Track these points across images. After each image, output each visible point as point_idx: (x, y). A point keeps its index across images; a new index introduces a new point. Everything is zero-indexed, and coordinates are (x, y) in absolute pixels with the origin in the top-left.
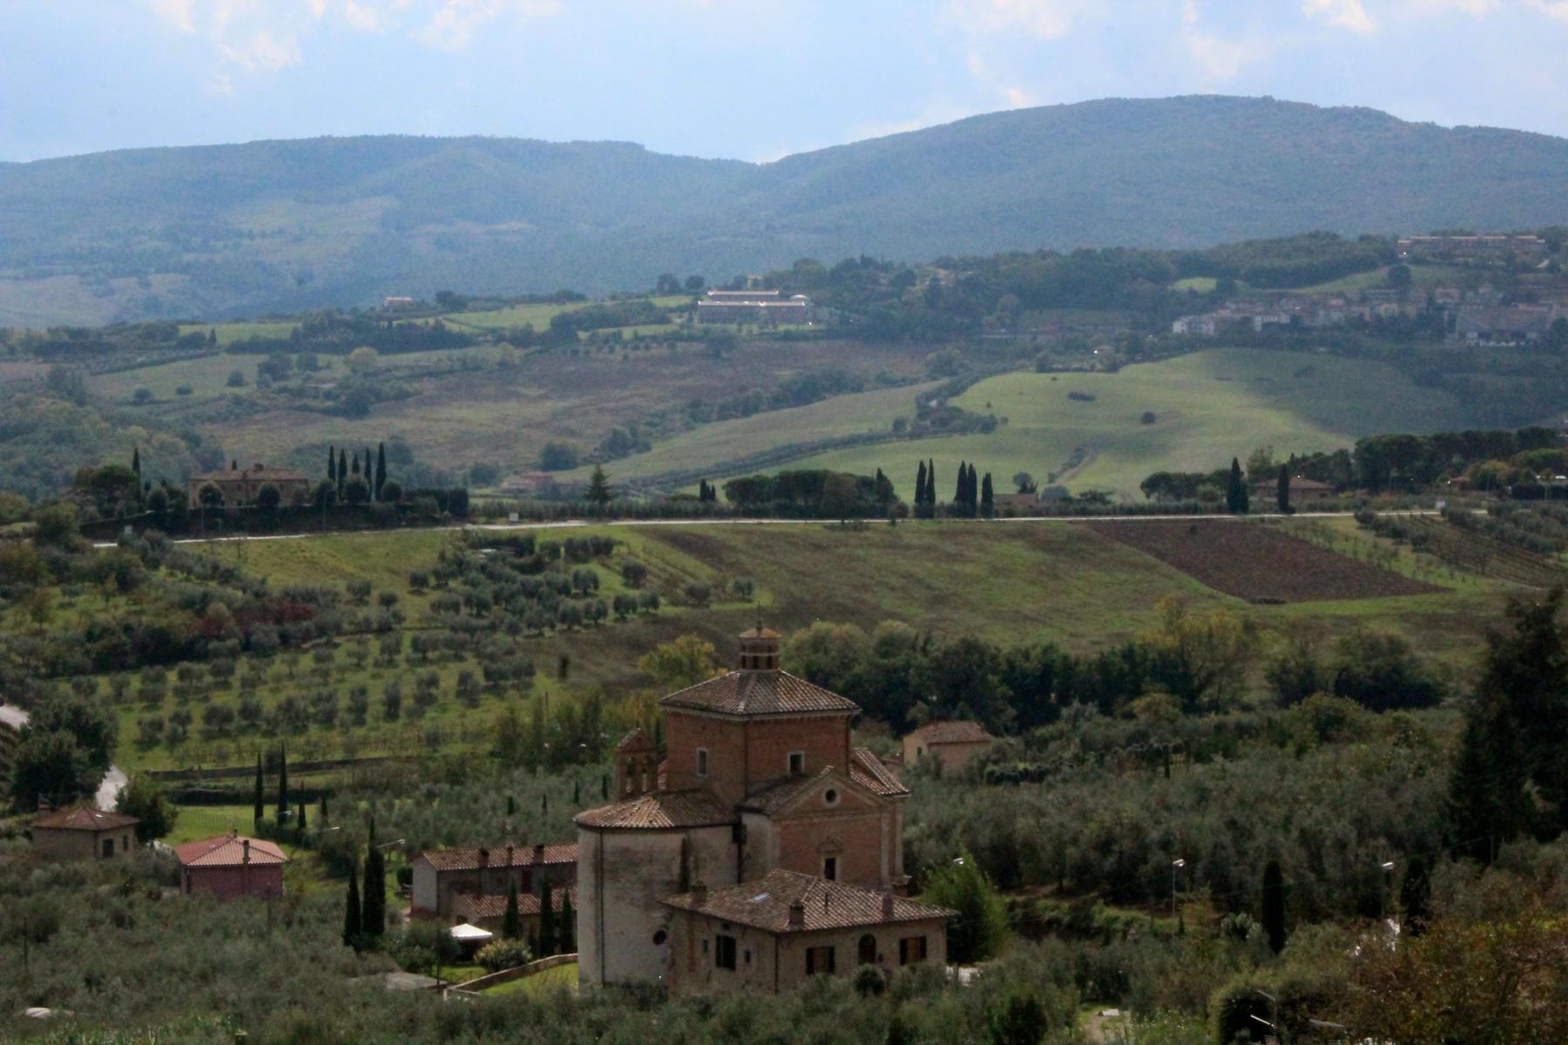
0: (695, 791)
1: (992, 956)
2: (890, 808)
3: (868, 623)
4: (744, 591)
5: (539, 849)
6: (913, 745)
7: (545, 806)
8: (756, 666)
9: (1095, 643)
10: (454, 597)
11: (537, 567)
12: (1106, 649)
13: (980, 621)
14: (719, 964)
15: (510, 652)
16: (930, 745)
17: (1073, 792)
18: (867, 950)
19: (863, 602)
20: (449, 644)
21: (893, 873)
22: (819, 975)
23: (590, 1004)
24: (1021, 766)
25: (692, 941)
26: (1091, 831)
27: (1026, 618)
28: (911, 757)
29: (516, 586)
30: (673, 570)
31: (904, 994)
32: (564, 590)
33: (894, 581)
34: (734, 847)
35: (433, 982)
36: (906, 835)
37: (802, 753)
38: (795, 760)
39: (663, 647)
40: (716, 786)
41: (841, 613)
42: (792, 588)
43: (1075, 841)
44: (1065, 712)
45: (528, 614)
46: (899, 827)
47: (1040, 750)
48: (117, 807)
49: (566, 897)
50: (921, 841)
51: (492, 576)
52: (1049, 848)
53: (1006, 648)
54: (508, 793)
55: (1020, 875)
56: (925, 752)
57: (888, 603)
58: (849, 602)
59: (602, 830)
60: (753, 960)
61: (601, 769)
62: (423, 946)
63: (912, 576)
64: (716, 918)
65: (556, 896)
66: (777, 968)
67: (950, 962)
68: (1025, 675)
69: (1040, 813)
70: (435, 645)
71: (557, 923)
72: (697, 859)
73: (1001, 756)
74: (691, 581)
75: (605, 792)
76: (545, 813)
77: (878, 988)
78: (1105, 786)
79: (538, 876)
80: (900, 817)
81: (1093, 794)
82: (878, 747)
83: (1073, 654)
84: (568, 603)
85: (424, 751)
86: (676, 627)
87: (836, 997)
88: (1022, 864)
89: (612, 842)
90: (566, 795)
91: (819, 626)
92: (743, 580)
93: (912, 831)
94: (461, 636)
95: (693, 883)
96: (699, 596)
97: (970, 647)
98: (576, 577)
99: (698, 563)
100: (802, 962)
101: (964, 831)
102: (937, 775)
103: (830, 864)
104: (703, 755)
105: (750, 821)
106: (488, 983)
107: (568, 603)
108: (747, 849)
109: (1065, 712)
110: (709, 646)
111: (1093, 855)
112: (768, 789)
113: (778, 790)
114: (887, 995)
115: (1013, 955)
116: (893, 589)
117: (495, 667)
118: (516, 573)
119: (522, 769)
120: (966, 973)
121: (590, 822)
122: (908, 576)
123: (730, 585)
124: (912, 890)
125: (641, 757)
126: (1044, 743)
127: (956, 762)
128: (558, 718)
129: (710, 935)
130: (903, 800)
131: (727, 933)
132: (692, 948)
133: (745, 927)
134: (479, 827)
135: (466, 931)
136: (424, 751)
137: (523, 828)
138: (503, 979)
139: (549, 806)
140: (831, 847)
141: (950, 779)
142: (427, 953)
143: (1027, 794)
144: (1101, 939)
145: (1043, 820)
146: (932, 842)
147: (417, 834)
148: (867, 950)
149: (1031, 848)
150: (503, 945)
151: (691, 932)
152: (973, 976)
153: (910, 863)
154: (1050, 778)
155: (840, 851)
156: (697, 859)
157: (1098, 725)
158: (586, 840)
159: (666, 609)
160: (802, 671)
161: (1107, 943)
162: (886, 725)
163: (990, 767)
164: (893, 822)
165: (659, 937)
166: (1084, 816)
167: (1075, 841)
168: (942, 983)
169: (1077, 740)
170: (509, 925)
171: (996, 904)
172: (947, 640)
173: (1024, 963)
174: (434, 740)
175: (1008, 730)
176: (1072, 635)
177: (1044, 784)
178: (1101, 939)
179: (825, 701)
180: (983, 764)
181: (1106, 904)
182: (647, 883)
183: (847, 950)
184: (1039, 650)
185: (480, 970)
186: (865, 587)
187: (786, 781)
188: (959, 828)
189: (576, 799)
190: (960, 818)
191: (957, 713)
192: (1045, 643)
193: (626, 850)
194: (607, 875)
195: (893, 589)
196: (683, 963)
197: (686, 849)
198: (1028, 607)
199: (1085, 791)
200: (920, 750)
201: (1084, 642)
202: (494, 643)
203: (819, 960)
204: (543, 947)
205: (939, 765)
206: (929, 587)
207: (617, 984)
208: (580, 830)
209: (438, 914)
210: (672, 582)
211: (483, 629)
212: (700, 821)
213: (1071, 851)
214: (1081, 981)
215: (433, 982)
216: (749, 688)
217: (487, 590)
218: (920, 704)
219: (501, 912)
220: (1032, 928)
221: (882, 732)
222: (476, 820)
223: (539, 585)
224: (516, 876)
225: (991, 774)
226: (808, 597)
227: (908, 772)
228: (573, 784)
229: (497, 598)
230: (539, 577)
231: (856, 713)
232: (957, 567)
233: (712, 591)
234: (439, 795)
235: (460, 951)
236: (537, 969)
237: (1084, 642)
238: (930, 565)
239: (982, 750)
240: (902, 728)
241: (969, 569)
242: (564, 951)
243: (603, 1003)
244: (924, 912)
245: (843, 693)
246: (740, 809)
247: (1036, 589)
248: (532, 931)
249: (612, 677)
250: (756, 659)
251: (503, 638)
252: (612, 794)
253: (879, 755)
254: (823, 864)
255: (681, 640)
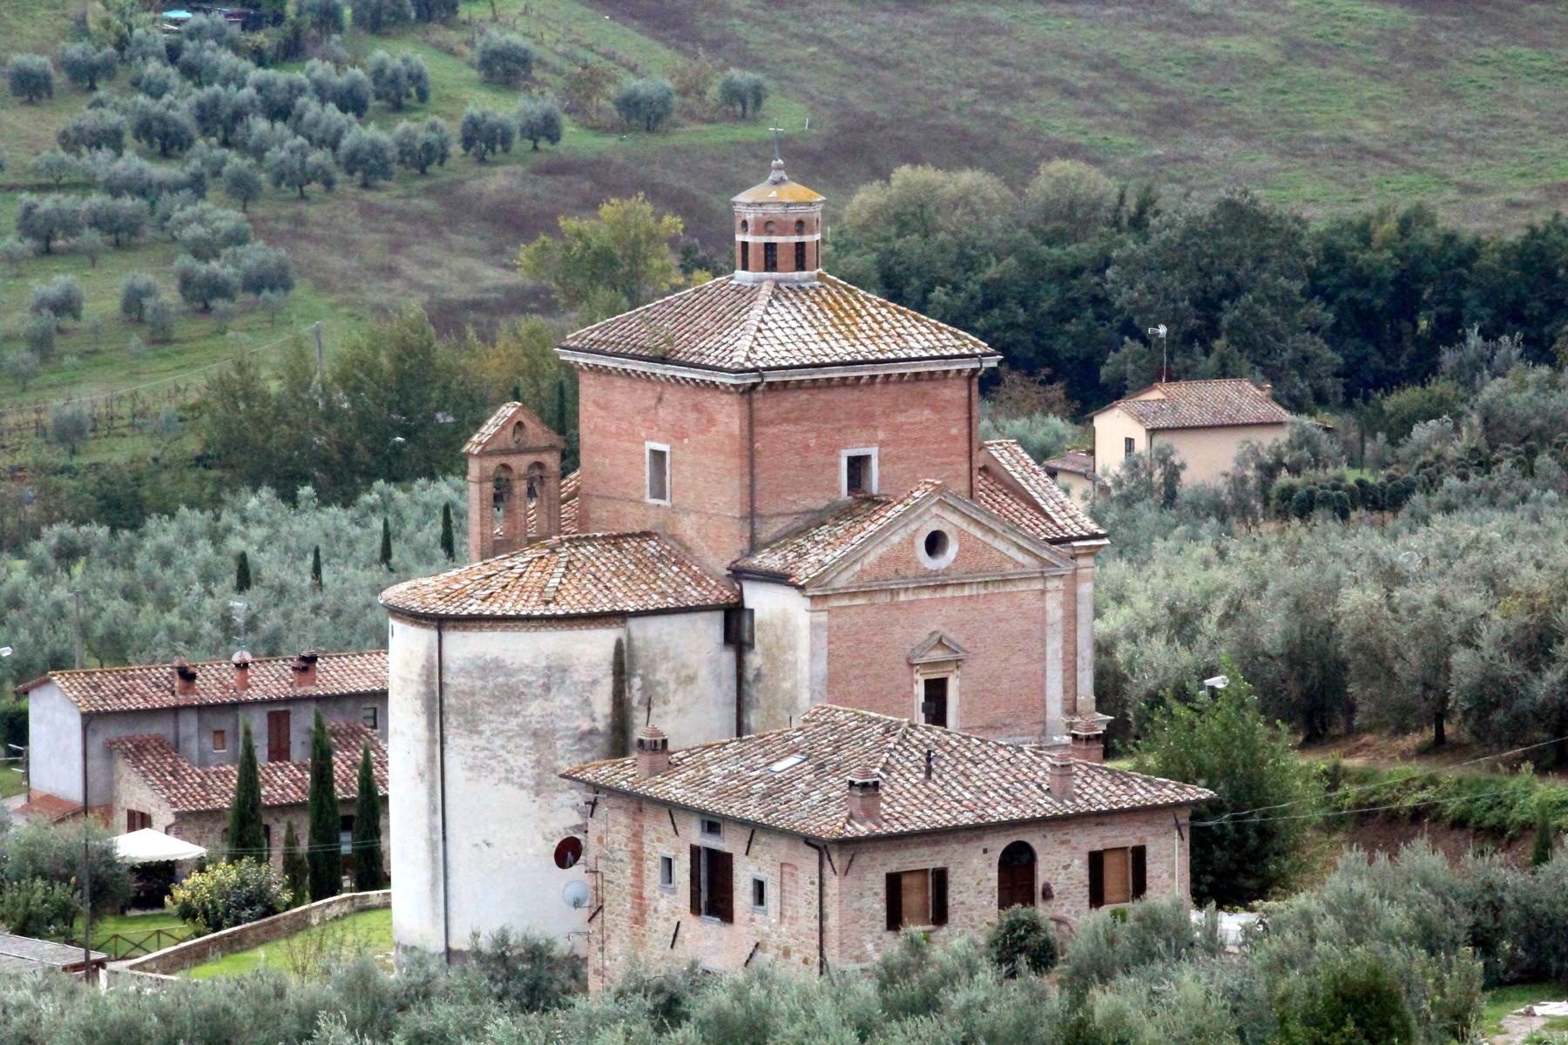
0: (646, 535)
1: (1290, 890)
2: (1066, 569)
3: (1017, 166)
4: (743, 103)
5: (307, 664)
6: (1116, 431)
7: (317, 570)
8: (770, 265)
9: (1514, 205)
10: (112, 118)
11: (292, 51)
12: (1540, 218)
13: (1265, 160)
14: (695, 909)
15: (237, 238)
16: (1152, 432)
17: (1463, 527)
18: (1017, 875)
19: (1004, 124)
20: (99, 221)
21: (1072, 710)
22: (916, 929)
23: (421, 993)
24: (1352, 476)
25: (638, 858)
26: (1501, 621)
27: (1363, 152)
28: (1110, 457)
29: (248, 92)
30: (591, 58)
31: (1098, 970)
32: (351, 102)
33: (1074, 75)
34: (728, 657)
35: (76, 955)
36: (1102, 627)
37: (873, 451)
38: (858, 465)
39: (569, 224)
40: (687, 527)
41: (961, 148)
42: (852, 96)
43: (1468, 638)
44: (1448, 357)
45: (275, 155)
46: (1085, 611)
47: (1393, 442)
48: (144, 514)
49: (366, 768)
50: (1133, 637)
51: (194, 73)
52: (1413, 655)
53: (1319, 219)
54: (235, 544)
55: (1351, 709)
56: (1141, 445)
57: (1060, 128)
58: (974, 126)
59: (441, 622)
60: (771, 893)
61: (443, 490)
62: (50, 876)
63: (1112, 63)
64: (687, 809)
65: (343, 767)
66: (822, 917)
67: (1199, 900)
68: (1361, 280)
69: (1392, 577)
70: (70, 226)
71: (347, 823)
72: (647, 686)
73: (1308, 452)
74: (631, 83)
75: (448, 543)
76: (319, 585)
77: (1044, 958)
78: (1536, 518)
79: (302, 723)
80: (1085, 589)
81: (1511, 535)
82: (1039, 437)
83: (1469, 229)
84: (364, 133)
85: (57, 456)
86: (602, 180)
87: (949, 978)
88: (1352, 689)
89: (463, 646)
90: (362, 551)
91: (904, 174)
92: (741, 76)
93: (1115, 621)
94: (128, 203)
95: (639, 732)
96: (643, 114)
97: (1237, 215)
98: (378, 73)
99: (645, 41)
100: (879, 907)
101: (1226, 620)
102: (1170, 498)
103: (936, 692)
104: (658, 456)
105: (758, 598)
106: (198, 956)
107: (364, 133)
108: (755, 660)
109: (1448, 357)
110: (672, 223)
111: (1510, 668)
112: (799, 533)
113: (823, 533)
114: (1060, 970)
115: (1336, 883)
116: (1070, 92)
117: (202, 269)
118: (247, 65)
119: (266, 493)
120: (1232, 924)
121: (416, 605)
122: (1104, 64)
123: (714, 92)
124: (1110, 744)
125: (520, 463)
126: (1400, 428)
127: (1208, 464)
128: (343, 379)
129: (676, 844)
130: (1092, 552)
131: (712, 842)
132: (638, 874)
133: (754, 829)
134: (173, 618)
135: (138, 847)
136: (57, 456)
137: (271, 621)
138: (234, 945)
139: (325, 570)
140: (938, 655)
141: (1195, 506)
142: (60, 892)
143: (1365, 538)
144: (1527, 849)
145: (1398, 593)
146: (1158, 643)
147: (35, 632)
148: (1017, 875)
149: (1378, 662)
150: (226, 874)
151: (636, 836)
152: (1247, 931)
153: (1109, 688)
154: (1417, 498)
155: (958, 663)
156: (647, 686)
157: (1523, 386)
158: (408, 647)
159: (575, 139)
160: (875, 275)
161: (1542, 857)
162: (1057, 391)
163: (1284, 478)
164: (1072, 598)
165: (568, 853)
166: (1493, 582)
167: (1468, 638)
168: (1181, 944)
169: (1476, 419)
170: (245, 828)
171: (1299, 767)
172: (1187, 203)
173: (1361, 901)
174: (70, 433)
175: (1321, 399)
176: (1467, 189)
177: (1403, 514)
178: (1527, 849)
179: (920, 338)
180: (1269, 471)
181: (1542, 770)
182: (540, 736)
183: (975, 880)
184: (1391, 226)
185: (180, 928)
186: (1010, 92)
187: (841, 513)
188: (1218, 608)
189: (386, 554)
190: (1222, 588)
191: (1212, 362)
192: (1402, 209)
193: (497, 666)
194: (452, 720)
195: (1070, 92)
196: (619, 908)
197: (622, 666)
198: (1369, 129)
199: (1494, 524)
200: (1129, 443)
201: (1492, 203)
202: (201, 219)
203: (914, 899)
204: (318, 876)
205: (1173, 474)
206: (1148, 88)
207: (478, 954)
208: (395, 625)
209: (86, 809)
210: (583, 86)
211: (175, 188)
212: (654, 601)
213: (1461, 658)
214: (1483, 941)
215: (76, 955)
216: (757, 311)
217: (181, 103)
218: (1131, 345)
219: (224, 802)
220: (1381, 824)
221: (1048, 407)
222: (165, 604)
223: (296, 90)
224: (258, 723)
225: (1287, 493)
226: (883, 112)
227: (1105, 490)
228: (377, 524)
229: (207, 116)
230: (297, 75)
231: (992, 363)
232: (1213, 44)
233: (676, 100)
234: (86, 551)
235: (133, 885)
236: (301, 924)
237: (1492, 203)
238: (1152, 38)
239: (1266, 440)
240: (1090, 394)
241: (1238, 45)
242: (361, 886)
243: (448, 994)
244: (1141, 794)
245: (959, 320)
246: (739, 574)
247: (1385, 89)
248: (291, 841)
249: (460, 292)
250: (770, 248)
251: (228, 217)
252: (471, 537)
253: (1041, 454)
254: (920, 690)
255: (610, 209)
